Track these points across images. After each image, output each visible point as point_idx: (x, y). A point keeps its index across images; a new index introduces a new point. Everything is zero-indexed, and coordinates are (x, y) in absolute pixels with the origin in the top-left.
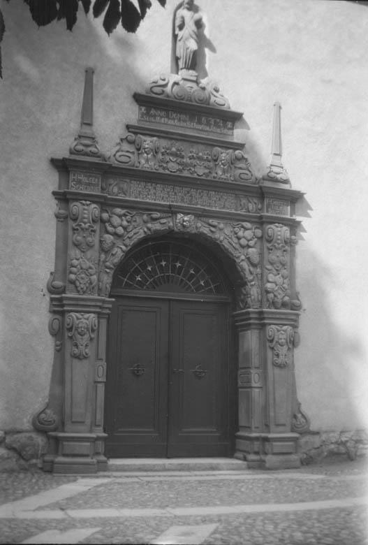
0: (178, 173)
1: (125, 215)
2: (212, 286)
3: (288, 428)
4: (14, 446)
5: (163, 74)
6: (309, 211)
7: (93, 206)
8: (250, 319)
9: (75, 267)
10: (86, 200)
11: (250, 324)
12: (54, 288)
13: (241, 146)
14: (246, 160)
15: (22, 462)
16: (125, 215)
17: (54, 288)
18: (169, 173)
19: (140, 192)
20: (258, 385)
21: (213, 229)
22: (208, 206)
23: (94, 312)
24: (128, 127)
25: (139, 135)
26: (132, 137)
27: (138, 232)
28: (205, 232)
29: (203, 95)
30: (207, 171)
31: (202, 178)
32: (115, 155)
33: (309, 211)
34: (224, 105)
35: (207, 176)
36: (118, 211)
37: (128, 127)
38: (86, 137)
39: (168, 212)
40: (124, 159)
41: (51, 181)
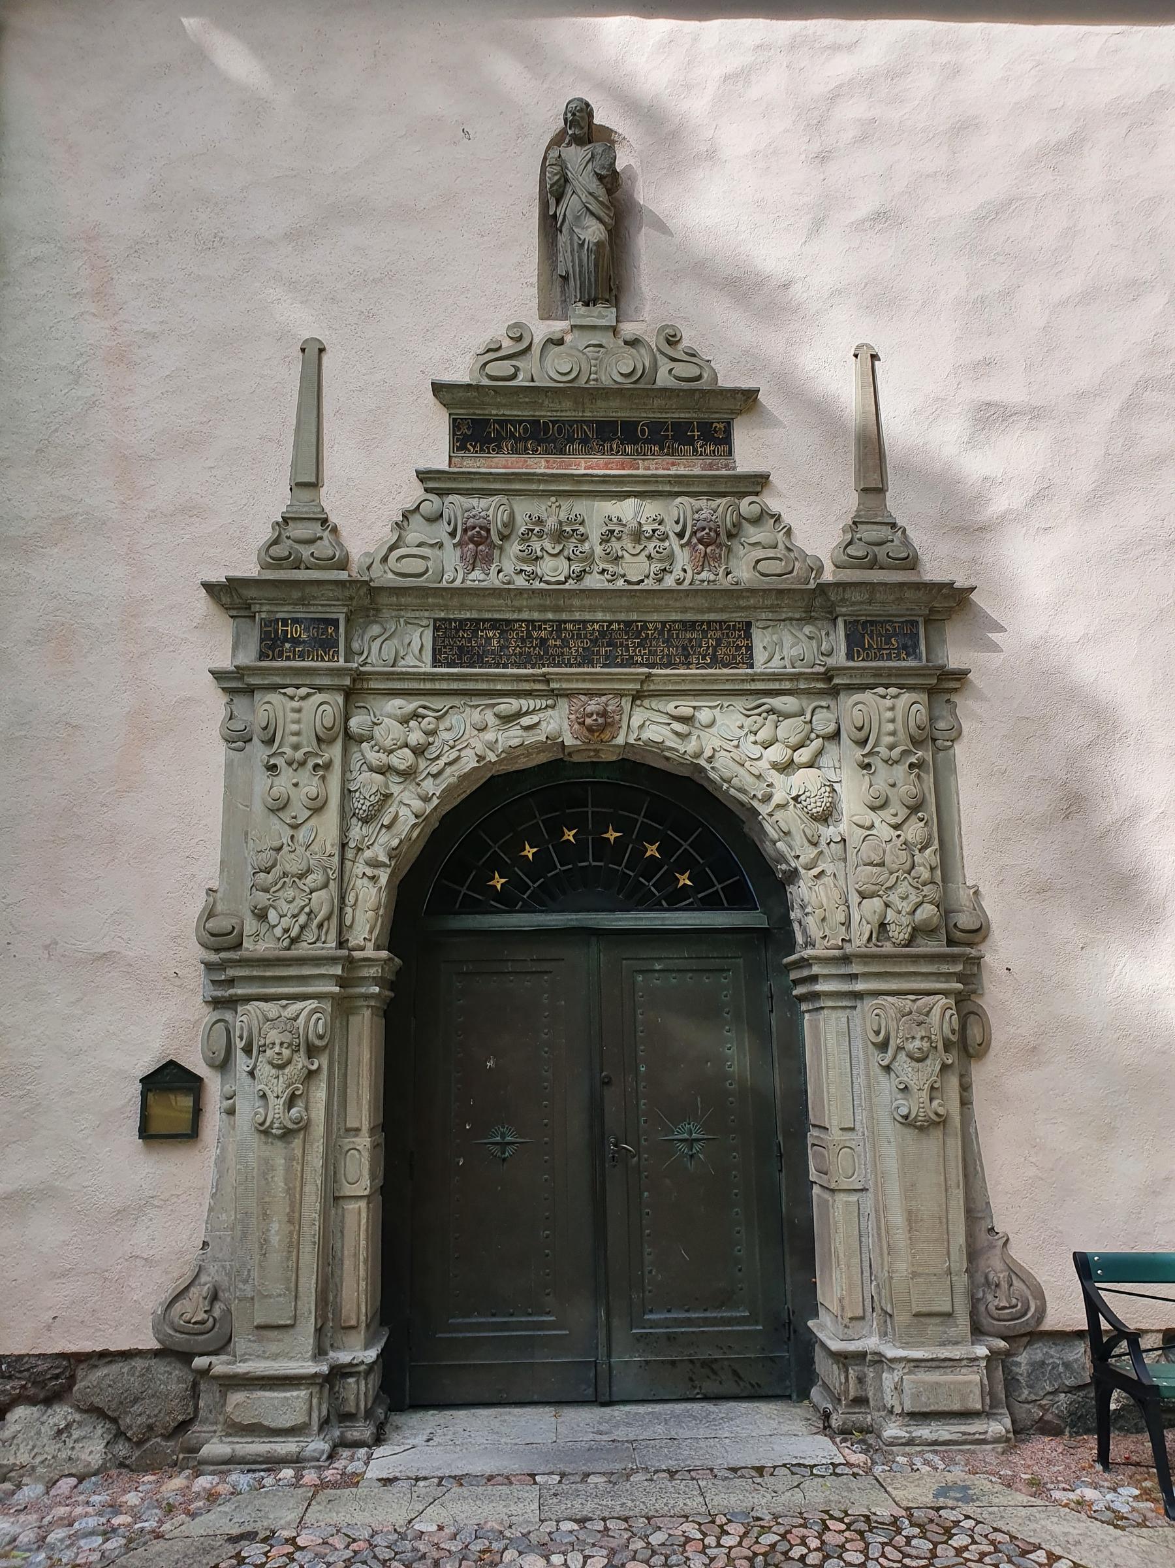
0: (571, 585)
1: (415, 716)
2: (464, 890)
3: (963, 1324)
4: (97, 1401)
5: (516, 325)
6: (995, 636)
7: (906, 697)
8: (814, 979)
9: (309, 871)
10: (887, 687)
11: (816, 996)
12: (213, 935)
13: (758, 482)
14: (778, 518)
15: (122, 1449)
16: (415, 716)
17: (213, 935)
18: (543, 586)
19: (460, 648)
20: (352, 1206)
21: (526, 721)
22: (666, 666)
23: (945, 993)
24: (424, 476)
25: (451, 498)
26: (433, 504)
27: (458, 758)
28: (515, 742)
29: (617, 367)
30: (576, 567)
31: (567, 586)
32: (385, 559)
33: (995, 636)
34: (700, 377)
35: (579, 578)
36: (396, 705)
37: (424, 476)
38: (306, 515)
39: (822, 693)
40: (416, 566)
41: (219, 645)
